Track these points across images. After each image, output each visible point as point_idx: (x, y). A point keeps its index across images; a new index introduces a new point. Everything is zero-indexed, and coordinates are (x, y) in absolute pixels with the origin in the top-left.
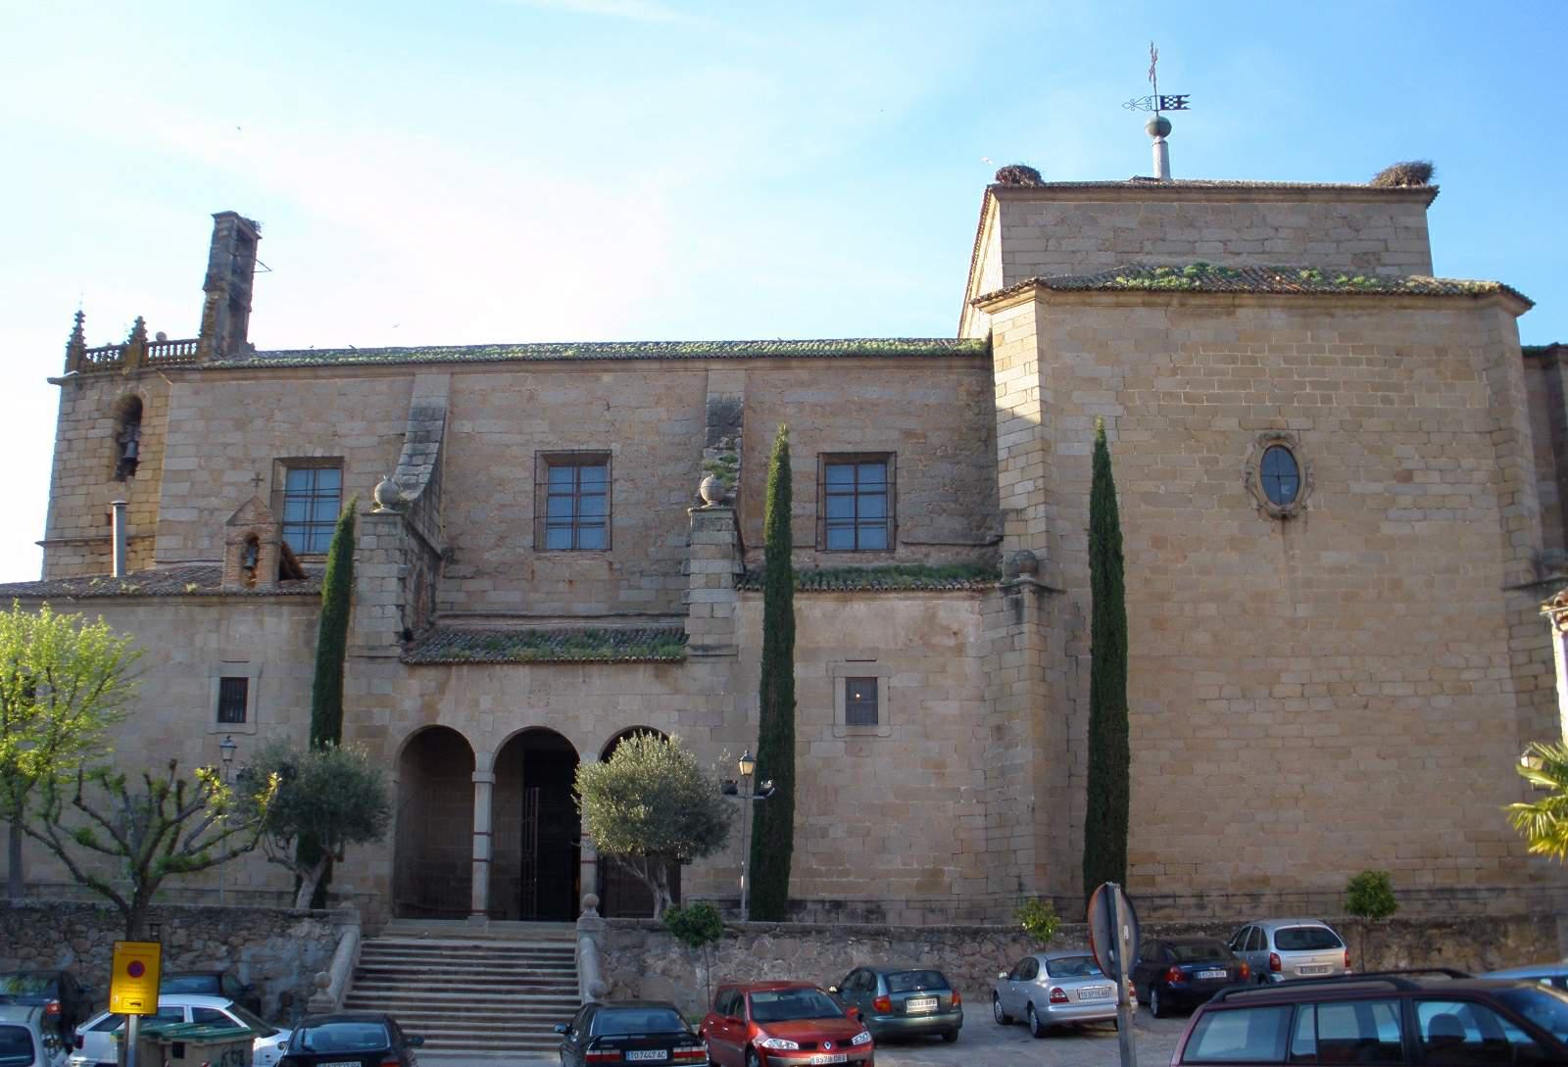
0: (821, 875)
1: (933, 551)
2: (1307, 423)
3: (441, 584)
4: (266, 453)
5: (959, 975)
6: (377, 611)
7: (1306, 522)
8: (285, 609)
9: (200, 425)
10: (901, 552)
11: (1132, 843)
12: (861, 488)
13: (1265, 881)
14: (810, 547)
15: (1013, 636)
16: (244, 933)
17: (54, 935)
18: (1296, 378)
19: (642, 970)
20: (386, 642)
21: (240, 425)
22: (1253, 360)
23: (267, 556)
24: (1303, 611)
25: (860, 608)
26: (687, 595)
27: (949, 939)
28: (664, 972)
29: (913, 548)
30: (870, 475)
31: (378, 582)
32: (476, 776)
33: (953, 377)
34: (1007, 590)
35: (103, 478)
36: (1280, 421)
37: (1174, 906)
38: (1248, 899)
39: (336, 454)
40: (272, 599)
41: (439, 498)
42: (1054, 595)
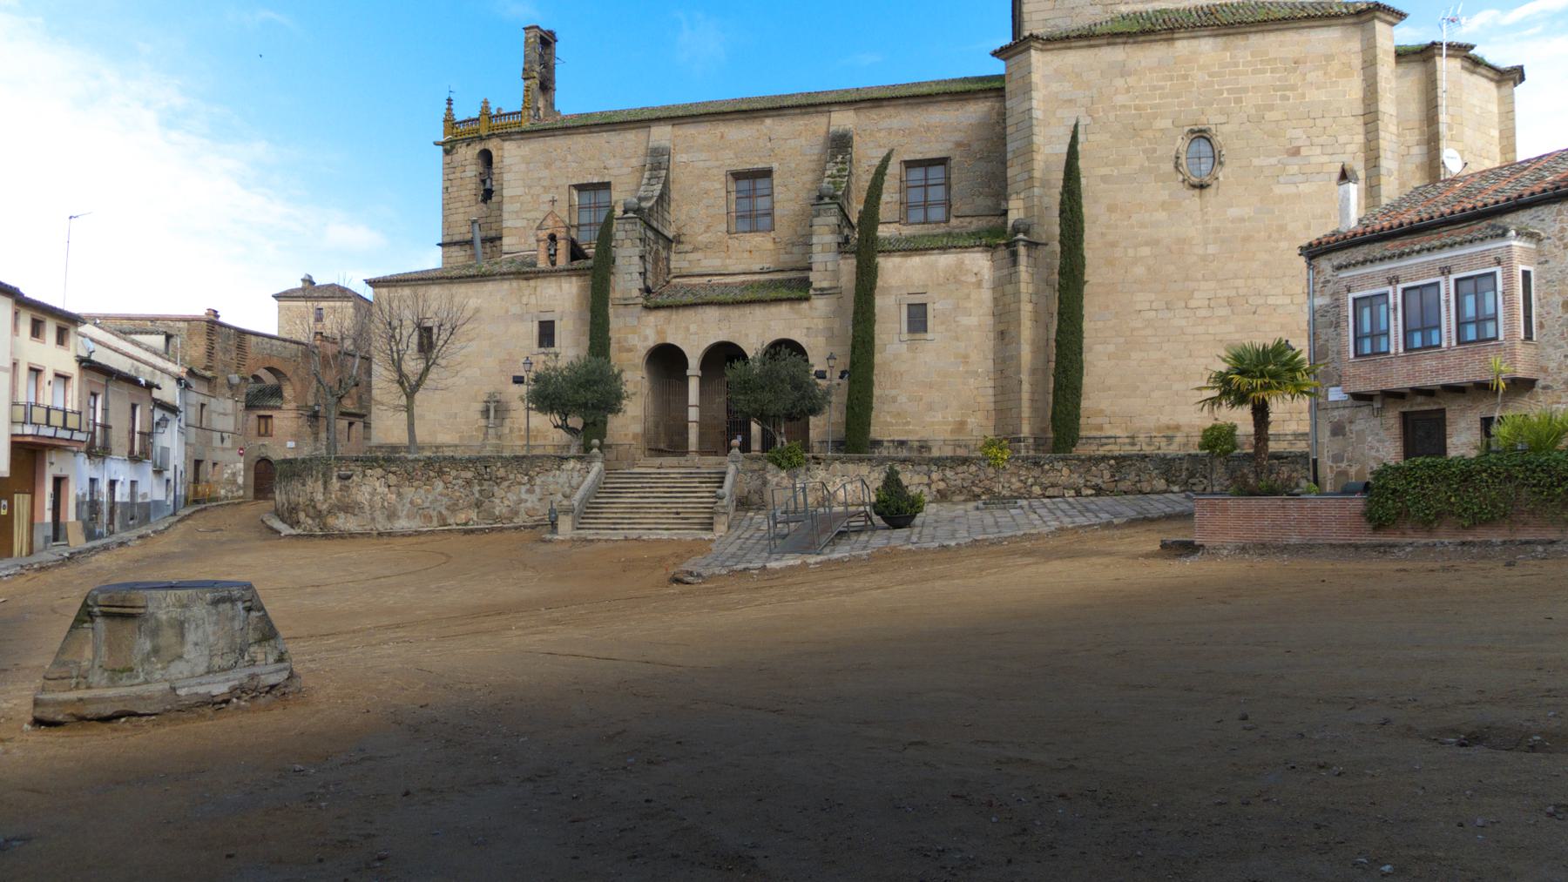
0: (892, 425)
1: (974, 220)
2: (1223, 119)
3: (673, 257)
4: (565, 182)
5: (955, 486)
6: (628, 277)
7: (1218, 188)
8: (574, 279)
10: (954, 222)
11: (1084, 404)
12: (930, 182)
13: (1177, 428)
16: (537, 469)
17: (432, 474)
18: (1216, 87)
19: (765, 483)
20: (634, 296)
21: (548, 165)
22: (1185, 77)
23: (562, 247)
24: (1212, 249)
25: (916, 260)
26: (810, 258)
27: (948, 463)
28: (777, 484)
30: (936, 173)
31: (627, 259)
32: (689, 372)
33: (989, 104)
34: (1007, 245)
35: (473, 203)
36: (1204, 119)
37: (1115, 443)
38: (1164, 439)
39: (606, 180)
40: (565, 273)
41: (669, 205)
42: (1039, 247)
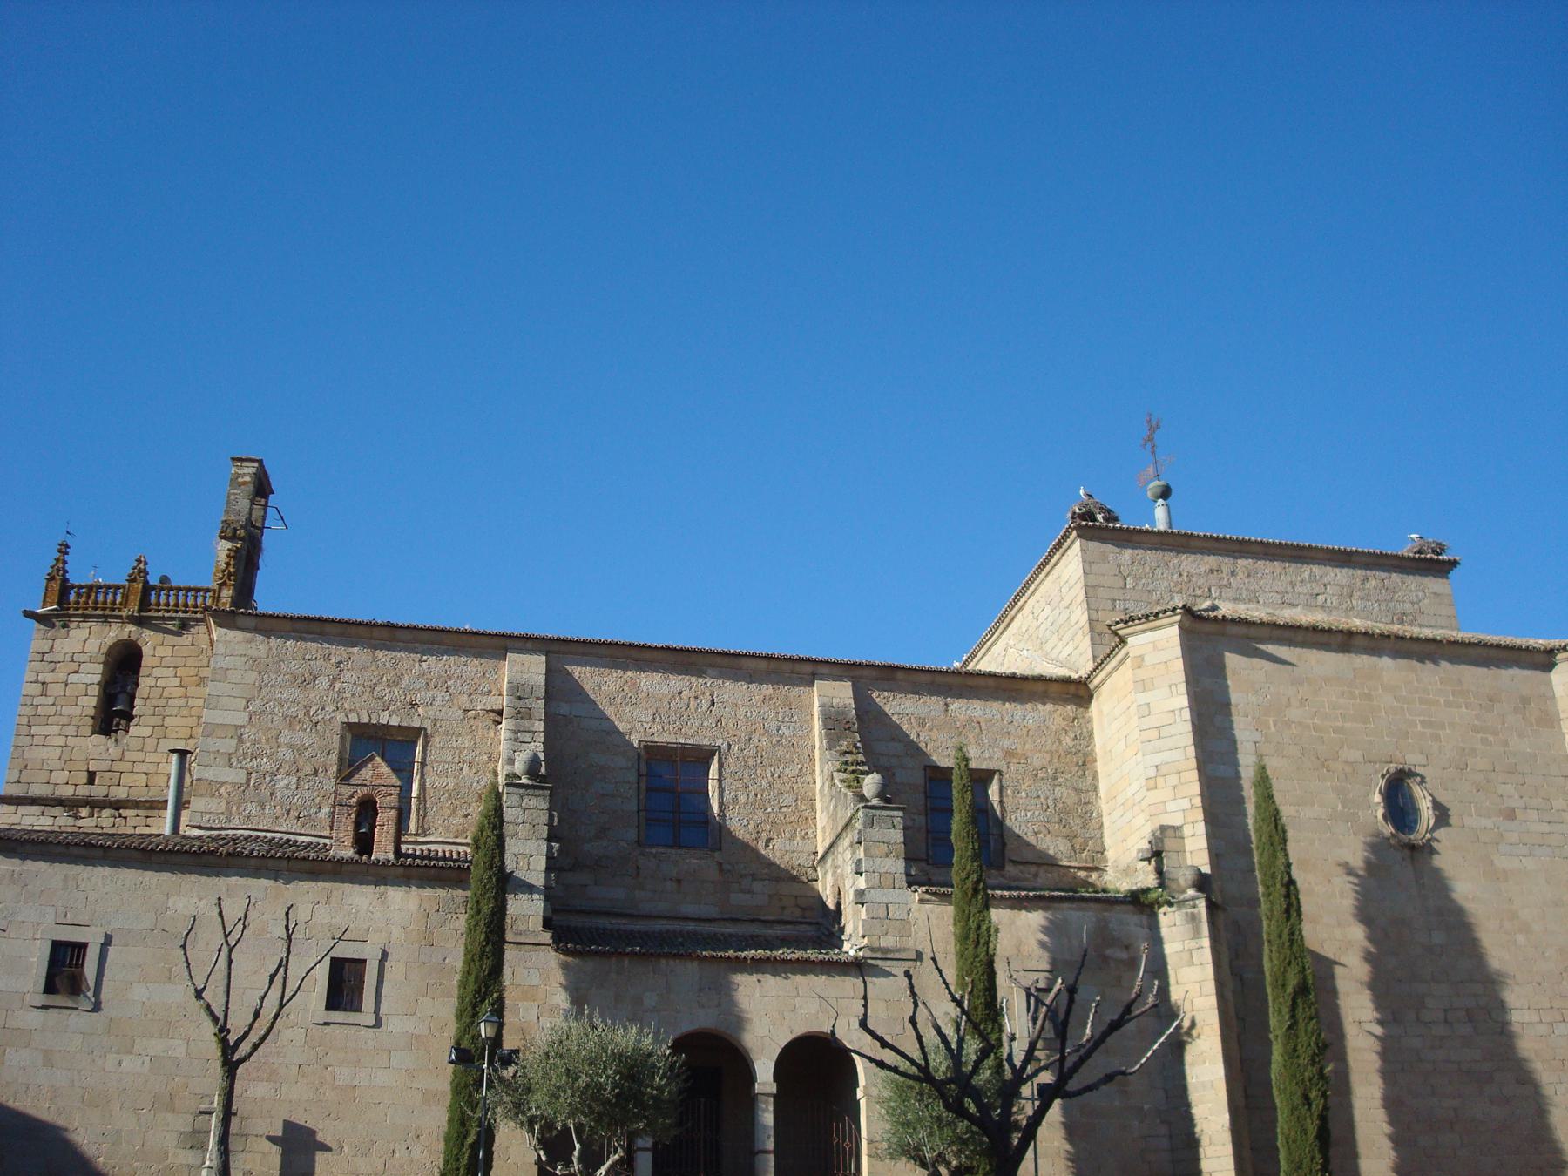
9: (253, 676)
14: (921, 860)
15: (1190, 950)
29: (1021, 867)
35: (88, 730)
